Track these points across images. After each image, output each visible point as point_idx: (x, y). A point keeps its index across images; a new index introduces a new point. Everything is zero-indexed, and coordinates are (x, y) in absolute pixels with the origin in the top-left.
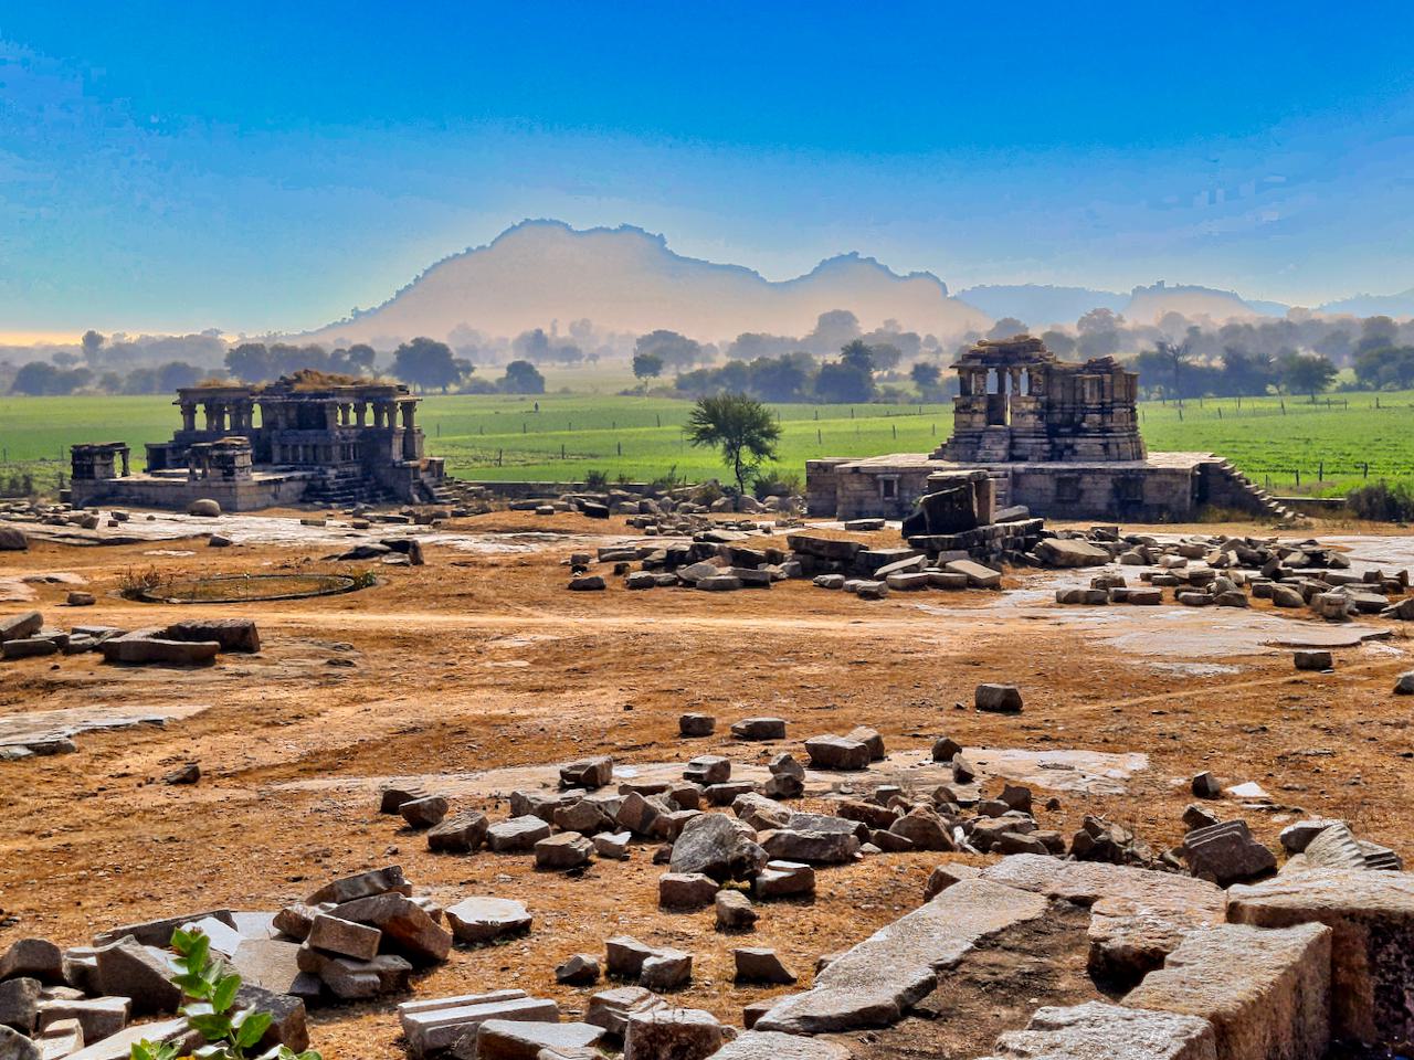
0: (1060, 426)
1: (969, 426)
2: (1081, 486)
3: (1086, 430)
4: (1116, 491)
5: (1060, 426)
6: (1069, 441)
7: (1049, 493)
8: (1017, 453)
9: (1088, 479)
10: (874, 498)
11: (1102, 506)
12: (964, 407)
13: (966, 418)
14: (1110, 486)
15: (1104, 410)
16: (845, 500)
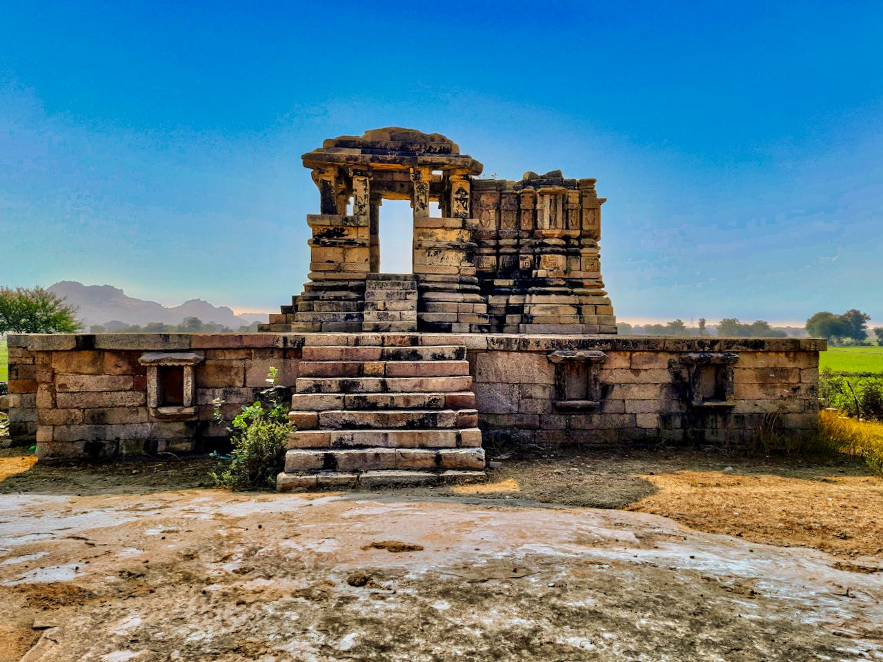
0: (494, 275)
1: (339, 269)
2: (607, 377)
3: (543, 282)
4: (680, 388)
5: (494, 275)
6: (514, 300)
7: (538, 392)
8: (430, 317)
9: (619, 361)
10: (134, 410)
11: (649, 422)
12: (329, 234)
13: (333, 254)
14: (666, 377)
15: (570, 249)
16: (58, 415)
